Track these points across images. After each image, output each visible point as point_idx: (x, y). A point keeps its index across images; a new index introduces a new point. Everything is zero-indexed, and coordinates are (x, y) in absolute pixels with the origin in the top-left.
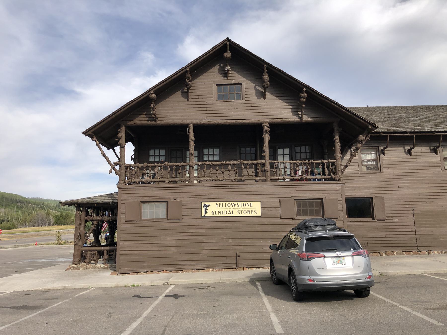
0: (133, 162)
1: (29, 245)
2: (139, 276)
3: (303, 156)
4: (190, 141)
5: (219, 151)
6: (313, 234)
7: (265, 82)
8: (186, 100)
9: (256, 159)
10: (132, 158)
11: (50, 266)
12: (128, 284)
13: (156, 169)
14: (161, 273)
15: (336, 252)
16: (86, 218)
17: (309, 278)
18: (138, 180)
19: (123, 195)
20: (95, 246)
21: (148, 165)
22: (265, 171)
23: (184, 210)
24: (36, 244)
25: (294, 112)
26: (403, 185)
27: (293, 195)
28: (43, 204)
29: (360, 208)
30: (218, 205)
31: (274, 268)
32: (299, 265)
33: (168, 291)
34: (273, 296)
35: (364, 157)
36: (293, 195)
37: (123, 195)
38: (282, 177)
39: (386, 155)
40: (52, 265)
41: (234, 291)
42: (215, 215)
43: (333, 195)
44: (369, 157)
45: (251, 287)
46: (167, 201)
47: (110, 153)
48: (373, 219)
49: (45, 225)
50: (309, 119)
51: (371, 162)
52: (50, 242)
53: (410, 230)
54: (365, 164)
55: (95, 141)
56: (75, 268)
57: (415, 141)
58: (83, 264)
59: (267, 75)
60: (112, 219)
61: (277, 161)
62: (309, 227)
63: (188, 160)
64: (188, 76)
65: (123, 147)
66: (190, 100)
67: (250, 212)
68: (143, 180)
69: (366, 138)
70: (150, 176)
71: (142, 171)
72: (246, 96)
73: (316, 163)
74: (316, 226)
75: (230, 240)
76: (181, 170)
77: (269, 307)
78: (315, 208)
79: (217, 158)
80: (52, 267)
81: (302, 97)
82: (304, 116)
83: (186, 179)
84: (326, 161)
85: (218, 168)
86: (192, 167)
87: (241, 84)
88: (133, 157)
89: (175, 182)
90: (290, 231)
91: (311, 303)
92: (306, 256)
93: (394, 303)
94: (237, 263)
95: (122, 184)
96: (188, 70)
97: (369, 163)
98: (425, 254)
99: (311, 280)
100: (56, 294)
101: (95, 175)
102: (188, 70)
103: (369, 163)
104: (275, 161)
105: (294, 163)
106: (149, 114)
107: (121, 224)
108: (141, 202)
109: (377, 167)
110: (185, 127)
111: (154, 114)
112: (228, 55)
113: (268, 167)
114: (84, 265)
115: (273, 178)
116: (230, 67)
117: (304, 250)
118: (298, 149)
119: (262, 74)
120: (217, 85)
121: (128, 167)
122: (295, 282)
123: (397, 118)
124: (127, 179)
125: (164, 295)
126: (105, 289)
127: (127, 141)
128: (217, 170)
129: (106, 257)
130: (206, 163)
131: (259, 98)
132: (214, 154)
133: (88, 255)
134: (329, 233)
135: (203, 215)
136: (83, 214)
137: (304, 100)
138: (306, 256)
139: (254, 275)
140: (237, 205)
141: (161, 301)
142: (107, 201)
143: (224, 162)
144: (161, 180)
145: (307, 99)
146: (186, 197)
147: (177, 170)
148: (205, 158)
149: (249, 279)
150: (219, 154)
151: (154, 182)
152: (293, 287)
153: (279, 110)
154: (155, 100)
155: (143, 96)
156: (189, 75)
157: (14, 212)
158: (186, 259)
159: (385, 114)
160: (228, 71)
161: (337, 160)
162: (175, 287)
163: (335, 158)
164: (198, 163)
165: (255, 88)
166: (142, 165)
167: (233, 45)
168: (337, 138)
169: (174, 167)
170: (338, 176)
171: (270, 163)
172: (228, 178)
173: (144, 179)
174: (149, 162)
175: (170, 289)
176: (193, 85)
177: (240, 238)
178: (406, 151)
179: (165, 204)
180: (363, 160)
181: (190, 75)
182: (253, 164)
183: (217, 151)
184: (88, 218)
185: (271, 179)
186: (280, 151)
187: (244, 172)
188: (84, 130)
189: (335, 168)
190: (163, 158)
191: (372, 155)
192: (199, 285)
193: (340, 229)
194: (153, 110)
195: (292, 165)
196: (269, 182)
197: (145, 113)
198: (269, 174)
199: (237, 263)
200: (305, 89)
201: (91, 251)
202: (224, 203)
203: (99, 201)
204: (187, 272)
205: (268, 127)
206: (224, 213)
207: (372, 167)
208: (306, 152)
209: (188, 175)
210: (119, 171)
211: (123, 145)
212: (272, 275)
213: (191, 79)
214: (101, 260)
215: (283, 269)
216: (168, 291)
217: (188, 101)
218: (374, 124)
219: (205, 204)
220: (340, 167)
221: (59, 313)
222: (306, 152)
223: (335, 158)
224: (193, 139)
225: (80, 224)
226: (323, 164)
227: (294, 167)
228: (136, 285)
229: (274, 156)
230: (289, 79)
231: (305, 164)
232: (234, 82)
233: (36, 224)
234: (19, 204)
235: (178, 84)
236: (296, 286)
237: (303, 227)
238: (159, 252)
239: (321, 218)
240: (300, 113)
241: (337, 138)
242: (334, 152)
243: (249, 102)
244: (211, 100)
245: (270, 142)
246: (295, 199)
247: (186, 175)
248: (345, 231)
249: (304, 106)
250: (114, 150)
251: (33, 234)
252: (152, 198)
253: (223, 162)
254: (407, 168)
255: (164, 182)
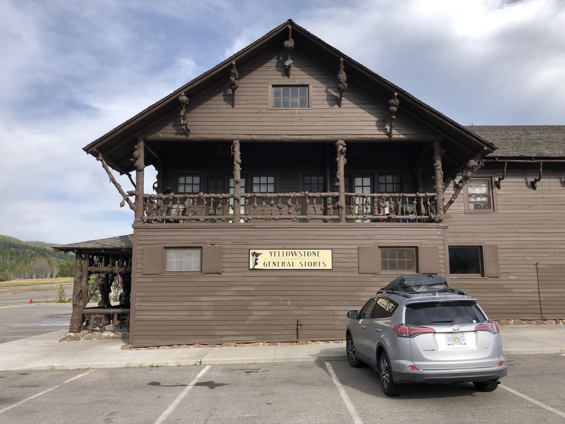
0: (155, 193)
1: (22, 303)
2: (161, 350)
3: (390, 188)
4: (235, 163)
5: (275, 180)
6: (417, 298)
7: (341, 83)
8: (230, 106)
9: (325, 191)
10: (154, 187)
11: (42, 333)
12: (144, 364)
13: (186, 203)
14: (191, 347)
15: (452, 325)
16: (89, 268)
17: (411, 363)
18: (161, 217)
19: (139, 238)
20: (103, 308)
21: (176, 196)
22: (338, 207)
23: (224, 260)
24: (31, 302)
25: (381, 125)
26: (523, 230)
27: (376, 241)
28: (45, 250)
29: (466, 260)
30: (273, 254)
31: (352, 343)
32: (395, 344)
33: (200, 375)
34: (353, 386)
35: (471, 190)
36: (376, 241)
37: (139, 238)
38: (362, 217)
39: (501, 188)
40: (45, 332)
41: (293, 376)
42: (268, 268)
43: (432, 242)
44: (478, 191)
45: (319, 371)
46: (201, 247)
47: (123, 180)
48: (483, 275)
49: (46, 277)
50: (401, 136)
51: (481, 198)
52: (50, 299)
53: (532, 291)
54: (473, 200)
55: (102, 161)
56: (73, 337)
57: (541, 170)
58: (85, 331)
59: (344, 73)
60: (125, 271)
61: (355, 194)
62: (409, 287)
63: (232, 191)
64: (233, 71)
65: (140, 171)
66: (236, 106)
67: (317, 264)
68: (167, 217)
69: (479, 163)
70: (178, 212)
71: (166, 206)
72: (314, 102)
73: (409, 198)
74: (419, 286)
75: (289, 303)
76: (222, 204)
77: (350, 407)
78: (406, 260)
79: (271, 188)
80: (43, 335)
81: (392, 105)
82: (394, 132)
83: (229, 217)
84: (423, 195)
85: (273, 202)
86: (237, 199)
87: (307, 86)
88: (156, 185)
89: (213, 221)
90: (378, 293)
91: (412, 400)
92: (408, 331)
93: (537, 403)
94: (298, 334)
95: (138, 222)
96: (234, 63)
97: (479, 199)
98: (551, 324)
99: (413, 367)
100: (39, 378)
101: (101, 209)
102: (234, 63)
103: (479, 199)
104: (353, 194)
105: (379, 197)
106: (177, 125)
107: (136, 279)
108: (165, 248)
109: (489, 205)
110: (227, 144)
111: (185, 125)
112: (290, 43)
113: (342, 202)
114: (85, 334)
115: (349, 217)
116: (292, 62)
117: (404, 322)
118: (382, 179)
119: (337, 72)
120: (273, 86)
121: (148, 199)
122: (389, 369)
123: (514, 140)
124: (146, 215)
125: (195, 381)
126: (111, 372)
127: (147, 164)
128: (272, 206)
129: (117, 322)
130: (257, 195)
131: (331, 105)
132: (267, 184)
133: (92, 320)
134: (439, 297)
135: (251, 267)
136: (85, 263)
137: (395, 109)
138: (408, 331)
139: (322, 352)
140: (298, 254)
141: (190, 393)
142: (118, 246)
143: (282, 195)
144: (193, 217)
145: (399, 107)
146: (228, 242)
147: (216, 204)
148: (255, 189)
149: (316, 358)
150: (275, 184)
151: (184, 220)
152: (384, 375)
153: (358, 122)
154: (187, 105)
155: (170, 99)
156: (234, 71)
157: (7, 259)
158: (226, 328)
159: (497, 135)
160: (289, 66)
161: (438, 193)
162: (210, 368)
163: (435, 191)
164: (245, 195)
165: (326, 91)
166: (166, 196)
167: (297, 30)
168: (438, 163)
169: (212, 199)
170: (439, 215)
171: (346, 196)
172: (288, 217)
173: (170, 215)
174: (177, 193)
175: (203, 372)
176: (240, 85)
177: (302, 299)
178: (529, 184)
179: (198, 251)
180: (470, 195)
181: (236, 70)
182: (322, 197)
183: (271, 180)
184: (93, 269)
185: (346, 219)
186: (358, 181)
187: (310, 209)
188: (85, 145)
189: (435, 204)
190: (196, 188)
191: (483, 188)
192: (245, 367)
193: (453, 291)
194: (184, 120)
195: (376, 200)
196: (344, 223)
197: (172, 124)
198: (343, 212)
199: (297, 335)
200: (396, 94)
201: (95, 314)
202: (281, 251)
203: (108, 245)
204: (227, 346)
205: (344, 146)
206: (280, 264)
207: (482, 205)
208: (393, 183)
209: (231, 212)
210: (135, 203)
211: (141, 167)
212: (348, 353)
213: (237, 75)
214: (110, 327)
215: (367, 346)
216: (200, 375)
217: (233, 107)
218: (492, 144)
219: (254, 252)
220: (441, 204)
221: (35, 412)
222: (393, 183)
223: (435, 191)
224: (240, 161)
225: (81, 277)
226: (419, 199)
227: (378, 202)
228: (155, 365)
229: (350, 187)
230: (373, 78)
231: (394, 198)
232: (297, 83)
233: (34, 275)
234: (13, 249)
235: (218, 83)
236: (390, 375)
237: (400, 287)
238: (188, 318)
239: (415, 273)
240: (388, 128)
241: (438, 163)
242: (434, 182)
243: (318, 111)
244: (266, 106)
245: (346, 167)
246: (379, 247)
247: (228, 211)
248: (463, 294)
249: (394, 117)
250: (130, 176)
251: (29, 287)
252: (181, 242)
253: (280, 194)
254: (529, 206)
255: (198, 220)
